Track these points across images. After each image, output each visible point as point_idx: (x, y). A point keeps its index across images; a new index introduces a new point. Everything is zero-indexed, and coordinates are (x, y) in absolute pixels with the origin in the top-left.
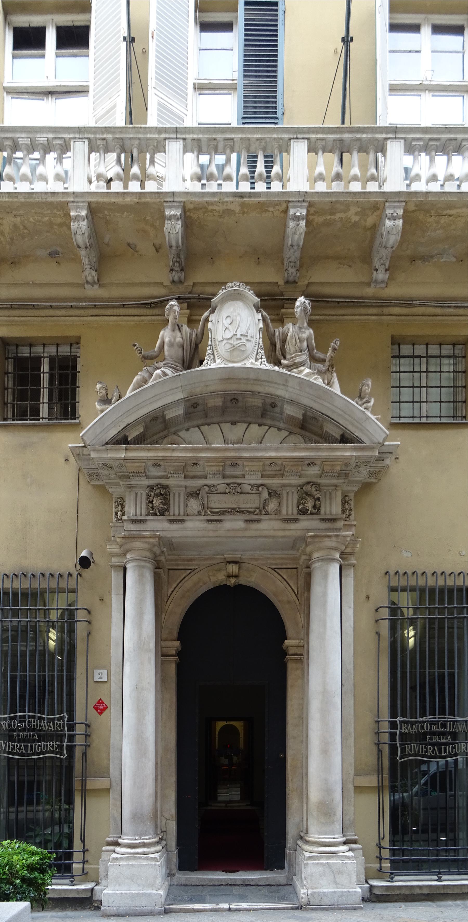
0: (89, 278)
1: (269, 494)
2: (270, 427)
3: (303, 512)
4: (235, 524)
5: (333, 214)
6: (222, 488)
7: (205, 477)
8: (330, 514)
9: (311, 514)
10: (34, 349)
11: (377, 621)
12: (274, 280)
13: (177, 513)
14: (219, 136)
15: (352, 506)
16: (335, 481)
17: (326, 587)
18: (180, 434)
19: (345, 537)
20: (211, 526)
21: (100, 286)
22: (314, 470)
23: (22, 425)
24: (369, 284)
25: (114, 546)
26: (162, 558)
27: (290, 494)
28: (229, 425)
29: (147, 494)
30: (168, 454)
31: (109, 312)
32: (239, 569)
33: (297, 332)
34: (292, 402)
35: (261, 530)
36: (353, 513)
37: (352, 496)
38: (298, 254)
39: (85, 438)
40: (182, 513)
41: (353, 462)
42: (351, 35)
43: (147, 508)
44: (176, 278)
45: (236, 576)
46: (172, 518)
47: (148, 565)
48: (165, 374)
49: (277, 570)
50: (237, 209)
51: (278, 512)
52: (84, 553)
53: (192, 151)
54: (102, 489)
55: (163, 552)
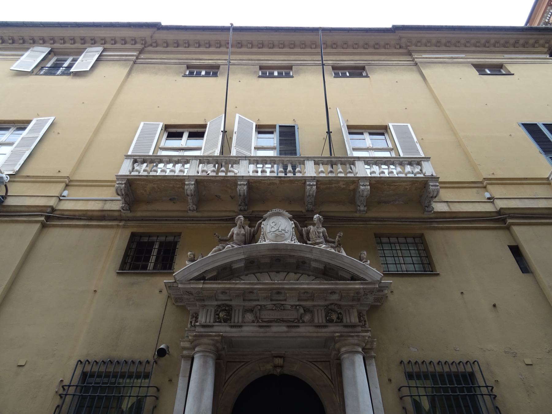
0: (191, 208)
1: (304, 310)
2: (302, 274)
3: (331, 321)
4: (279, 329)
5: (332, 184)
6: (269, 307)
7: (258, 300)
8: (351, 322)
9: (336, 322)
10: (151, 238)
11: (401, 398)
12: (300, 210)
13: (236, 321)
14: (268, 159)
15: (366, 319)
16: (351, 303)
17: (354, 371)
18: (241, 277)
19: (364, 336)
20: (262, 330)
21: (197, 212)
22: (335, 297)
23: (134, 273)
24: (356, 212)
25: (186, 343)
26: (223, 353)
27: (320, 311)
28: (274, 273)
29: (215, 310)
30: (232, 286)
31: (202, 222)
32: (284, 361)
33: (316, 229)
34: (316, 260)
35: (299, 332)
36: (367, 323)
37: (365, 313)
38: (313, 199)
39: (176, 277)
40: (240, 320)
41: (362, 291)
42: (330, 131)
43: (215, 318)
44: (242, 208)
45: (282, 367)
46: (233, 324)
47: (211, 355)
48: (233, 247)
49: (315, 363)
50: (278, 182)
51: (312, 321)
52: (162, 346)
53: (253, 164)
54: (183, 308)
55: (224, 348)
